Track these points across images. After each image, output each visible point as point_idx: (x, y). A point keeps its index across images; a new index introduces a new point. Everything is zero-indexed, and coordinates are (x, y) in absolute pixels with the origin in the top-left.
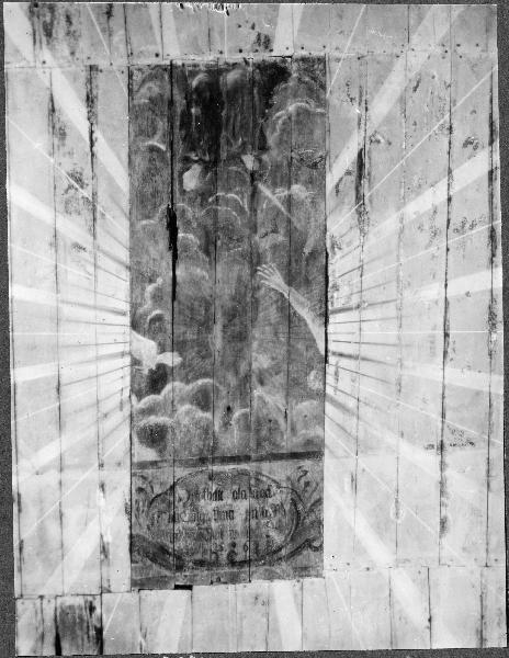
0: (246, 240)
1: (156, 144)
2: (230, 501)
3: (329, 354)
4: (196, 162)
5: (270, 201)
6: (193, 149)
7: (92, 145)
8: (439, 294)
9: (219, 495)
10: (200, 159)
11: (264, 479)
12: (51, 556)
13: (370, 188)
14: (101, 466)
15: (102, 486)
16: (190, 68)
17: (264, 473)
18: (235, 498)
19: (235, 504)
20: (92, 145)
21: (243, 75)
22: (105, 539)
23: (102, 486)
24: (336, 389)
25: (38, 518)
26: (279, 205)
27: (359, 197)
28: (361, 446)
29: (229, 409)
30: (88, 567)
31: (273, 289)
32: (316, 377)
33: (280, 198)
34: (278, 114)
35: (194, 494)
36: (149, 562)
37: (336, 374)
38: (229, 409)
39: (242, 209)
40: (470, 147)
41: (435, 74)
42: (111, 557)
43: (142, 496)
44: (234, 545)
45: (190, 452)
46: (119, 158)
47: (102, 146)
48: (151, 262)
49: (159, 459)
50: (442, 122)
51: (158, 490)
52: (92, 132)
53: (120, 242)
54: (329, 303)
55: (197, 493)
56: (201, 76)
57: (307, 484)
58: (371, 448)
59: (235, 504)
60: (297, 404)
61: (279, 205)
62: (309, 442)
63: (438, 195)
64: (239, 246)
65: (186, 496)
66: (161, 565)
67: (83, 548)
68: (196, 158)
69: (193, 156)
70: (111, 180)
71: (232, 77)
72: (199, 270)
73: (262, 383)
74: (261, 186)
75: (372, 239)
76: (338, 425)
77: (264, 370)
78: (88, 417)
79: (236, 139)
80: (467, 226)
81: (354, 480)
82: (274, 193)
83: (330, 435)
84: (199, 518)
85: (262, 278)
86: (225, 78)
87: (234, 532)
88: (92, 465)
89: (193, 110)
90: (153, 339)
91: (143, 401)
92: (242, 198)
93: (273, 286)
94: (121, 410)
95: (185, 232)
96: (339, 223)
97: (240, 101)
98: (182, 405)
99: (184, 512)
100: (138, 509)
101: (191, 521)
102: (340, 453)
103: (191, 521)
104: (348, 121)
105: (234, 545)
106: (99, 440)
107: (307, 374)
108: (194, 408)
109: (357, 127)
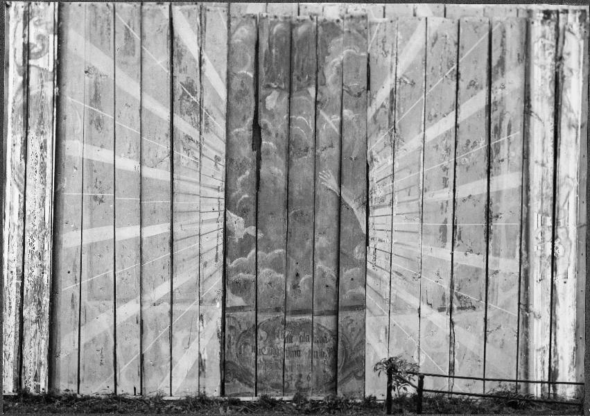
0: (311, 151)
1: (245, 72)
2: (297, 343)
3: (370, 240)
4: (276, 88)
5: (328, 124)
6: (273, 81)
7: (200, 65)
8: (449, 197)
9: (290, 339)
10: (279, 87)
11: (323, 329)
12: (163, 366)
13: (399, 117)
14: (200, 302)
15: (201, 317)
16: (272, 19)
17: (323, 324)
18: (300, 342)
19: (301, 346)
20: (200, 65)
21: (309, 28)
22: (203, 357)
23: (201, 317)
24: (374, 265)
25: (155, 338)
26: (333, 126)
27: (393, 127)
28: (394, 306)
29: (297, 275)
30: (189, 376)
31: (330, 189)
32: (359, 251)
33: (334, 122)
34: (334, 60)
35: (272, 334)
36: (237, 382)
37: (375, 253)
38: (297, 275)
39: (308, 127)
40: (472, 88)
41: (447, 34)
42: (206, 371)
43: (233, 332)
44: (300, 376)
45: (269, 303)
46: (219, 73)
47: (208, 68)
48: (244, 79)
49: (245, 305)
50: (452, 68)
51: (244, 327)
52: (201, 56)
53: (220, 138)
54: (370, 202)
55: (274, 333)
56: (279, 26)
57: (353, 330)
58: (400, 309)
59: (301, 346)
60: (346, 270)
61: (333, 126)
62: (354, 298)
63: (447, 124)
64: (306, 155)
65: (266, 336)
66: (246, 383)
67: (185, 363)
68: (275, 86)
69: (273, 85)
70: (215, 94)
71: (301, 30)
72: (276, 169)
73: (322, 258)
74: (321, 112)
75: (400, 154)
76: (376, 292)
77: (323, 248)
78: (194, 264)
79: (304, 77)
80: (471, 144)
81: (388, 332)
82: (331, 118)
83: (370, 299)
84: (274, 352)
85: (322, 181)
86: (296, 31)
87: (300, 367)
88: (194, 300)
89: (274, 51)
90: (242, 296)
91: (235, 262)
92: (308, 120)
93: (330, 187)
94: (216, 261)
95: (267, 140)
96: (377, 144)
97: (307, 47)
98: (263, 268)
99: (264, 348)
100: (230, 342)
101: (269, 354)
102: (377, 312)
103: (269, 354)
104: (383, 67)
105: (300, 376)
106: (200, 282)
107: (353, 249)
108: (272, 271)
109: (389, 73)
